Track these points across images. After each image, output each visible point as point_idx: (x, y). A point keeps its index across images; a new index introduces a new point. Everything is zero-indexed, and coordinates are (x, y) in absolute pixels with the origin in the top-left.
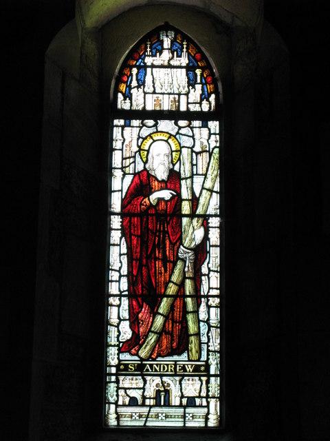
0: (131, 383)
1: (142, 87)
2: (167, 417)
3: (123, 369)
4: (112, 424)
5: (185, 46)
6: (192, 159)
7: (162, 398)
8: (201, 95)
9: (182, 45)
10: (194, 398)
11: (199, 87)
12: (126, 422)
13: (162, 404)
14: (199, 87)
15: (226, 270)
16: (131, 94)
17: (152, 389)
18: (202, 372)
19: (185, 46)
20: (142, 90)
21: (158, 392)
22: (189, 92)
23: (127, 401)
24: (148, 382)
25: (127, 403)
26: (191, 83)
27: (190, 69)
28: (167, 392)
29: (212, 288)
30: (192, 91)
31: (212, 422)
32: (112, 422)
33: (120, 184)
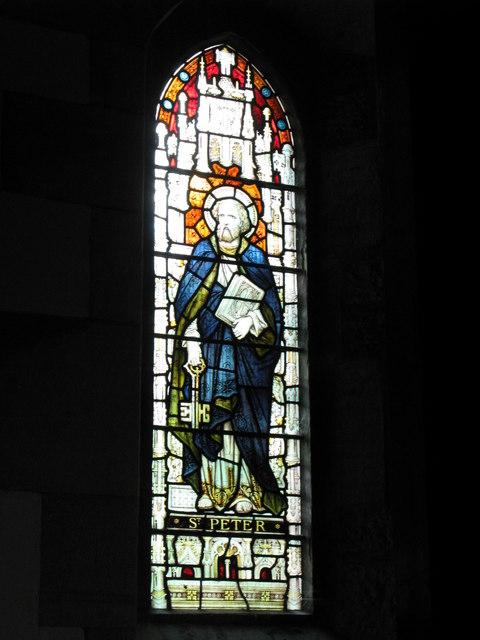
0: (188, 550)
1: (194, 121)
2: (223, 595)
3: (177, 525)
4: (160, 607)
5: (249, 75)
6: (284, 294)
7: (228, 568)
8: (272, 144)
9: (245, 73)
10: (274, 575)
11: (267, 130)
12: (179, 604)
13: (228, 576)
14: (267, 130)
15: (317, 395)
16: (178, 129)
17: (213, 555)
18: (277, 531)
19: (249, 75)
20: (193, 125)
21: (221, 560)
22: (255, 138)
23: (187, 575)
24: (207, 544)
25: (179, 575)
26: (259, 127)
27: (257, 106)
28: (234, 559)
29: (195, 190)
30: (259, 137)
31: (294, 605)
32: (159, 603)
33: (168, 270)
